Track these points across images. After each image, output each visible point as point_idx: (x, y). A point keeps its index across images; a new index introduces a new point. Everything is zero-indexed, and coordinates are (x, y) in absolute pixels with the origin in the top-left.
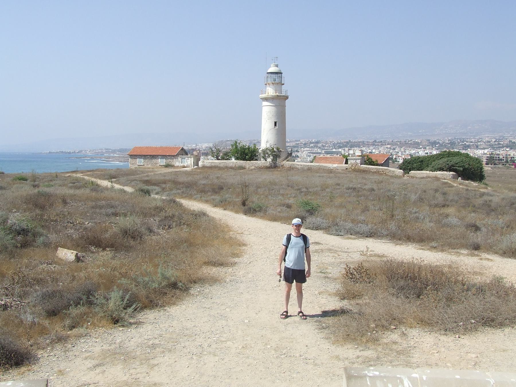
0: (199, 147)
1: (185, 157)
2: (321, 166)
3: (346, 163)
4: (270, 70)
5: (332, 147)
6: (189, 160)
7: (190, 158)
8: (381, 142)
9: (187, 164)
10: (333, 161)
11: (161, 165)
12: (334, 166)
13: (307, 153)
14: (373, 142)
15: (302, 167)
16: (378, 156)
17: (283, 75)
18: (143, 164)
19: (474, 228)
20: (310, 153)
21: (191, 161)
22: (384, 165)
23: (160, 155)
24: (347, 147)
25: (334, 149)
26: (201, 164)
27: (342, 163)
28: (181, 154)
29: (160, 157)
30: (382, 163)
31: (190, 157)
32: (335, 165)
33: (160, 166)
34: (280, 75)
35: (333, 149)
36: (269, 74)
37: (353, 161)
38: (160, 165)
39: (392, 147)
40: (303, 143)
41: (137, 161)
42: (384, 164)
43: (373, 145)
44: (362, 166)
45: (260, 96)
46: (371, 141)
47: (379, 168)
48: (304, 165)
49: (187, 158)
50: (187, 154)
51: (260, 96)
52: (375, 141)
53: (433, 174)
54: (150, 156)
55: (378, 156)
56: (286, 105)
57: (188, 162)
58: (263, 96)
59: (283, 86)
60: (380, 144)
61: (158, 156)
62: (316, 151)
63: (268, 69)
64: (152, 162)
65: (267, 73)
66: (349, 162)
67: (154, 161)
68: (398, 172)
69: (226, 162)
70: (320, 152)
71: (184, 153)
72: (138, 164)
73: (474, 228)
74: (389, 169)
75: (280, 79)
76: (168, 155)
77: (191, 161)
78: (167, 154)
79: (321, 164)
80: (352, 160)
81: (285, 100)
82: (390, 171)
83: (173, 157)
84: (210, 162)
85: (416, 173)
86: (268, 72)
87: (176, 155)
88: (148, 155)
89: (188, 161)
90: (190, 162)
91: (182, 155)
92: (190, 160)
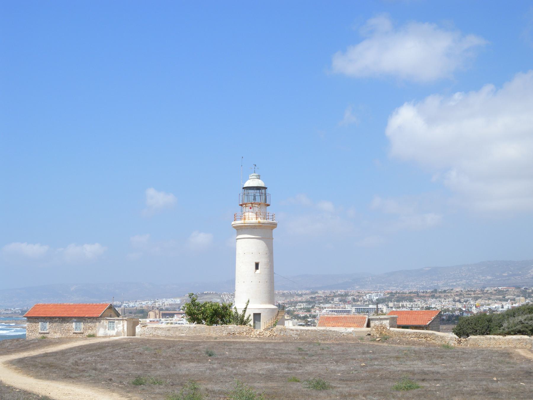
0: (160, 305)
1: (114, 320)
2: (327, 332)
3: (368, 326)
4: (248, 184)
5: (369, 302)
6: (120, 324)
7: (122, 321)
8: (445, 291)
9: (117, 331)
10: (346, 323)
11: (76, 333)
12: (348, 330)
13: (328, 312)
14: (432, 292)
15: (298, 333)
16: (422, 313)
17: (268, 191)
18: (48, 332)
19: (158, 394)
20: (332, 311)
21: (123, 325)
22: (434, 328)
23: (75, 317)
24: (391, 302)
25: (371, 304)
26: (139, 330)
27: (362, 327)
28: (109, 314)
29: (75, 320)
30: (427, 324)
31: (123, 320)
32: (350, 330)
33: (75, 334)
34: (263, 191)
35: (369, 304)
36: (246, 190)
37: (377, 323)
38: (74, 333)
39: (463, 299)
40: (322, 297)
41: (39, 326)
42: (430, 325)
43: (433, 297)
44: (392, 329)
45: (233, 223)
46: (429, 291)
47: (419, 333)
48: (301, 330)
49: (117, 321)
50: (118, 315)
51: (233, 223)
52: (435, 291)
53: (505, 339)
54: (59, 318)
55: (422, 313)
56: (273, 237)
57: (119, 328)
58: (239, 222)
59: (268, 207)
60: (443, 295)
61: (71, 318)
62: (342, 308)
63: (245, 183)
64: (62, 328)
65: (244, 188)
66: (372, 324)
67: (66, 325)
68: (449, 339)
69: (179, 327)
70: (349, 309)
71: (113, 314)
72: (40, 331)
73: (158, 394)
74: (435, 334)
75: (264, 197)
76: (87, 317)
77: (123, 325)
78: (86, 316)
79: (328, 328)
80: (377, 321)
81: (272, 230)
82: (437, 336)
83: (340, 344)
84: (152, 328)
85: (478, 340)
86: (245, 186)
87: (101, 317)
88: (55, 318)
89: (118, 326)
90: (122, 328)
91: (111, 317)
92: (122, 324)
